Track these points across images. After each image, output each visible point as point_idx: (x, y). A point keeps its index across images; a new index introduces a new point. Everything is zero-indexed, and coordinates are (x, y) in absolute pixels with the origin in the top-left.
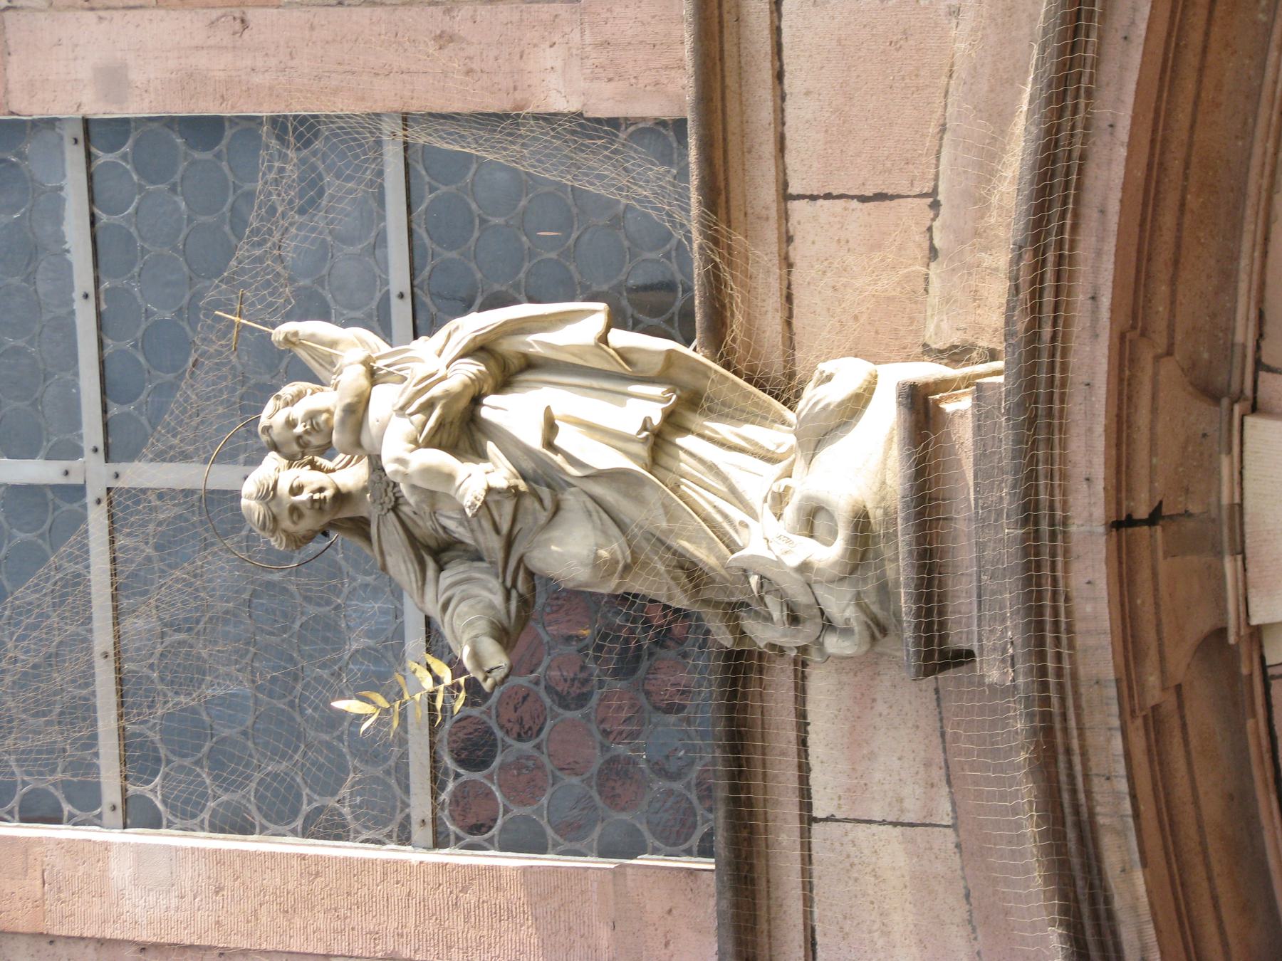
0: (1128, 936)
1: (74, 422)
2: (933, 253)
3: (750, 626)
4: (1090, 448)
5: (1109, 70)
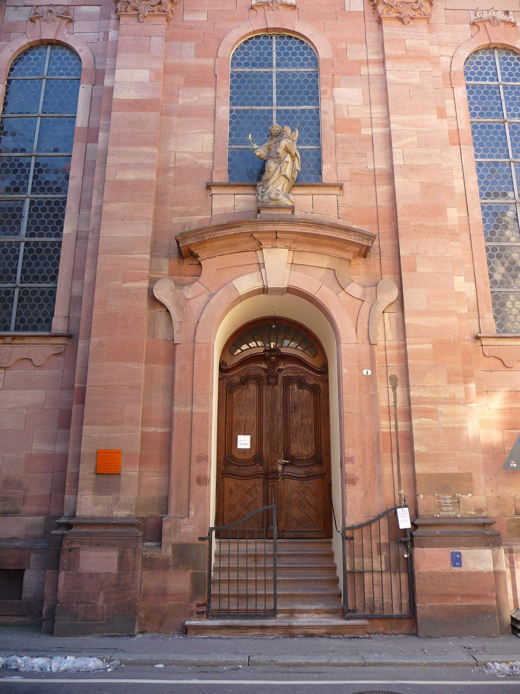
0: (225, 231)
1: (281, 105)
2: (306, 213)
3: (261, 187)
4: (287, 229)
5: (333, 232)
